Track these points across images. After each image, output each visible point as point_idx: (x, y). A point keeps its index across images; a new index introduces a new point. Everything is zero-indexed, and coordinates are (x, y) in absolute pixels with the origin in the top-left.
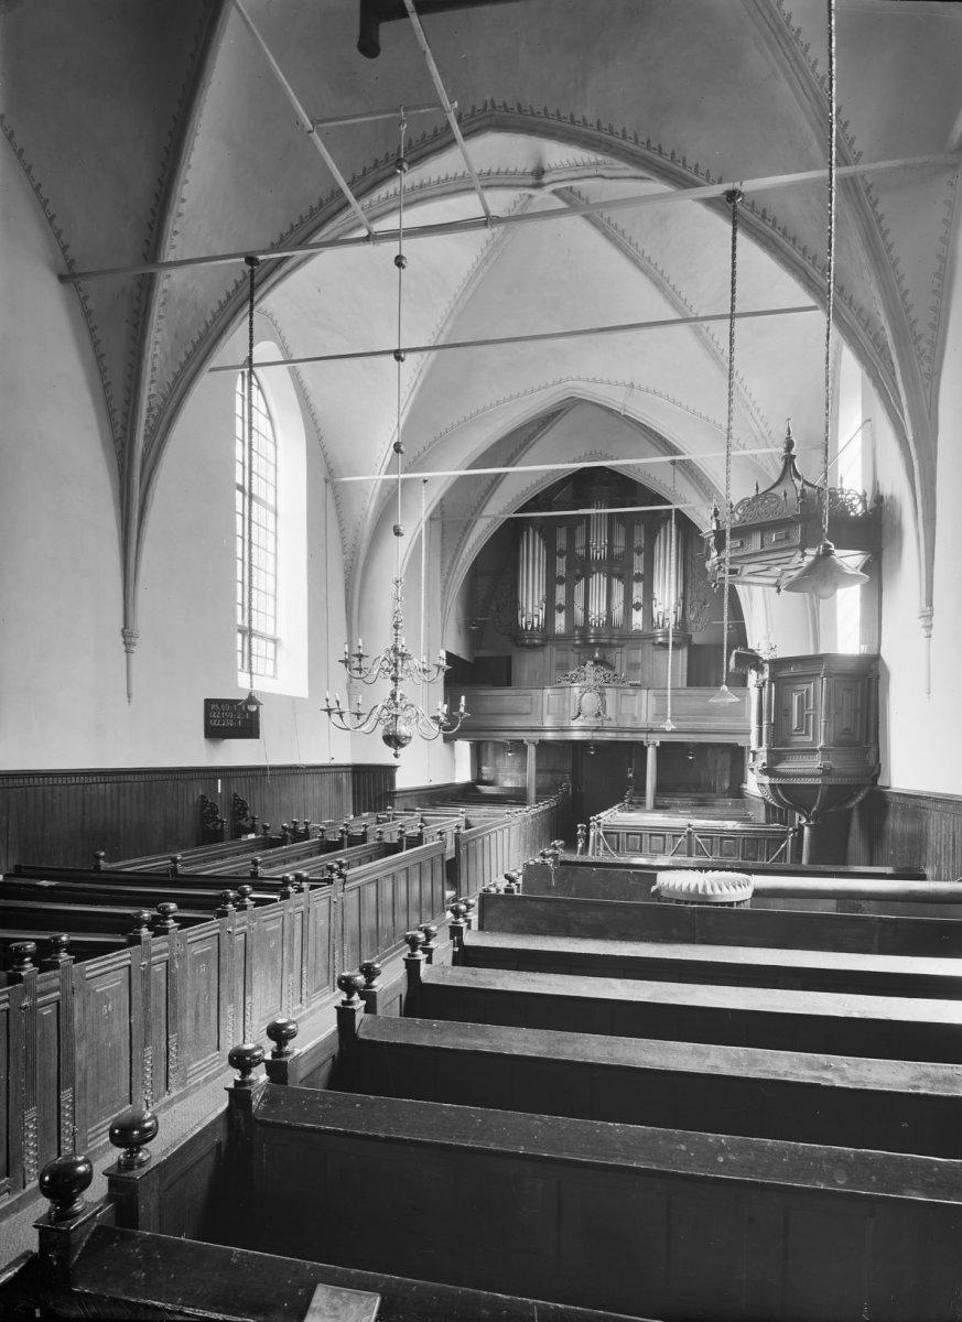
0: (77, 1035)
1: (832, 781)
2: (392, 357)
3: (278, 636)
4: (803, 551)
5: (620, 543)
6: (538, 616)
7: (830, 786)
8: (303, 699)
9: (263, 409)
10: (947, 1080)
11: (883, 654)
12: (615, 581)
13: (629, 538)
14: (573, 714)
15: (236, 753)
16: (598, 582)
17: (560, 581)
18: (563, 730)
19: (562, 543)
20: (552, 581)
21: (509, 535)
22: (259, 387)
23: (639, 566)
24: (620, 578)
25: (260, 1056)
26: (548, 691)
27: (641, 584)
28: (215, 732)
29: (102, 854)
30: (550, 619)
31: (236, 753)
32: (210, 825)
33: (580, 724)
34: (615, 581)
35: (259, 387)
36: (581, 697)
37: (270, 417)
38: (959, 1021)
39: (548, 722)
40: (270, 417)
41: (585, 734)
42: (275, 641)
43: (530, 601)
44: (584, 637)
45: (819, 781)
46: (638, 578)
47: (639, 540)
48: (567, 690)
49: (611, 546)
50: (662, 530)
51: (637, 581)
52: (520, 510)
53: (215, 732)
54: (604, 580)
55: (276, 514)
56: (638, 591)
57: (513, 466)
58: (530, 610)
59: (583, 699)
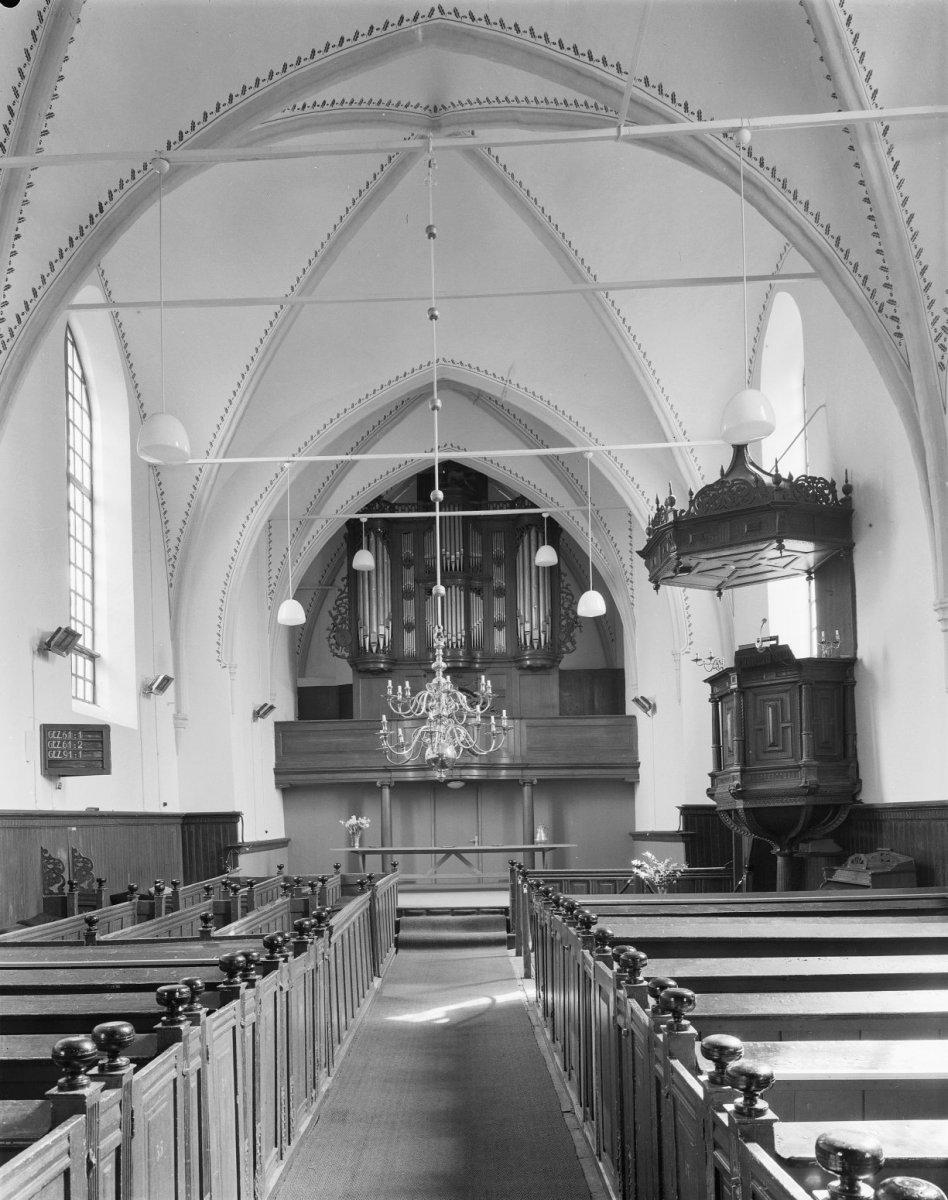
0: (20, 1113)
1: (820, 801)
3: (97, 651)
4: (780, 541)
5: (477, 554)
6: (384, 635)
7: (815, 807)
8: (133, 730)
9: (78, 371)
11: (859, 656)
12: (473, 596)
13: (486, 547)
15: (80, 794)
17: (408, 595)
19: (408, 551)
21: (352, 535)
22: (74, 344)
23: (499, 580)
24: (479, 592)
27: (502, 600)
28: (55, 768)
30: (397, 638)
31: (80, 794)
32: (55, 889)
35: (74, 344)
37: (84, 380)
40: (84, 380)
42: (93, 657)
43: (374, 617)
45: (799, 803)
46: (500, 592)
47: (498, 549)
49: (466, 556)
51: (499, 596)
53: (55, 768)
55: (92, 499)
56: (499, 611)
57: (364, 453)
58: (375, 630)
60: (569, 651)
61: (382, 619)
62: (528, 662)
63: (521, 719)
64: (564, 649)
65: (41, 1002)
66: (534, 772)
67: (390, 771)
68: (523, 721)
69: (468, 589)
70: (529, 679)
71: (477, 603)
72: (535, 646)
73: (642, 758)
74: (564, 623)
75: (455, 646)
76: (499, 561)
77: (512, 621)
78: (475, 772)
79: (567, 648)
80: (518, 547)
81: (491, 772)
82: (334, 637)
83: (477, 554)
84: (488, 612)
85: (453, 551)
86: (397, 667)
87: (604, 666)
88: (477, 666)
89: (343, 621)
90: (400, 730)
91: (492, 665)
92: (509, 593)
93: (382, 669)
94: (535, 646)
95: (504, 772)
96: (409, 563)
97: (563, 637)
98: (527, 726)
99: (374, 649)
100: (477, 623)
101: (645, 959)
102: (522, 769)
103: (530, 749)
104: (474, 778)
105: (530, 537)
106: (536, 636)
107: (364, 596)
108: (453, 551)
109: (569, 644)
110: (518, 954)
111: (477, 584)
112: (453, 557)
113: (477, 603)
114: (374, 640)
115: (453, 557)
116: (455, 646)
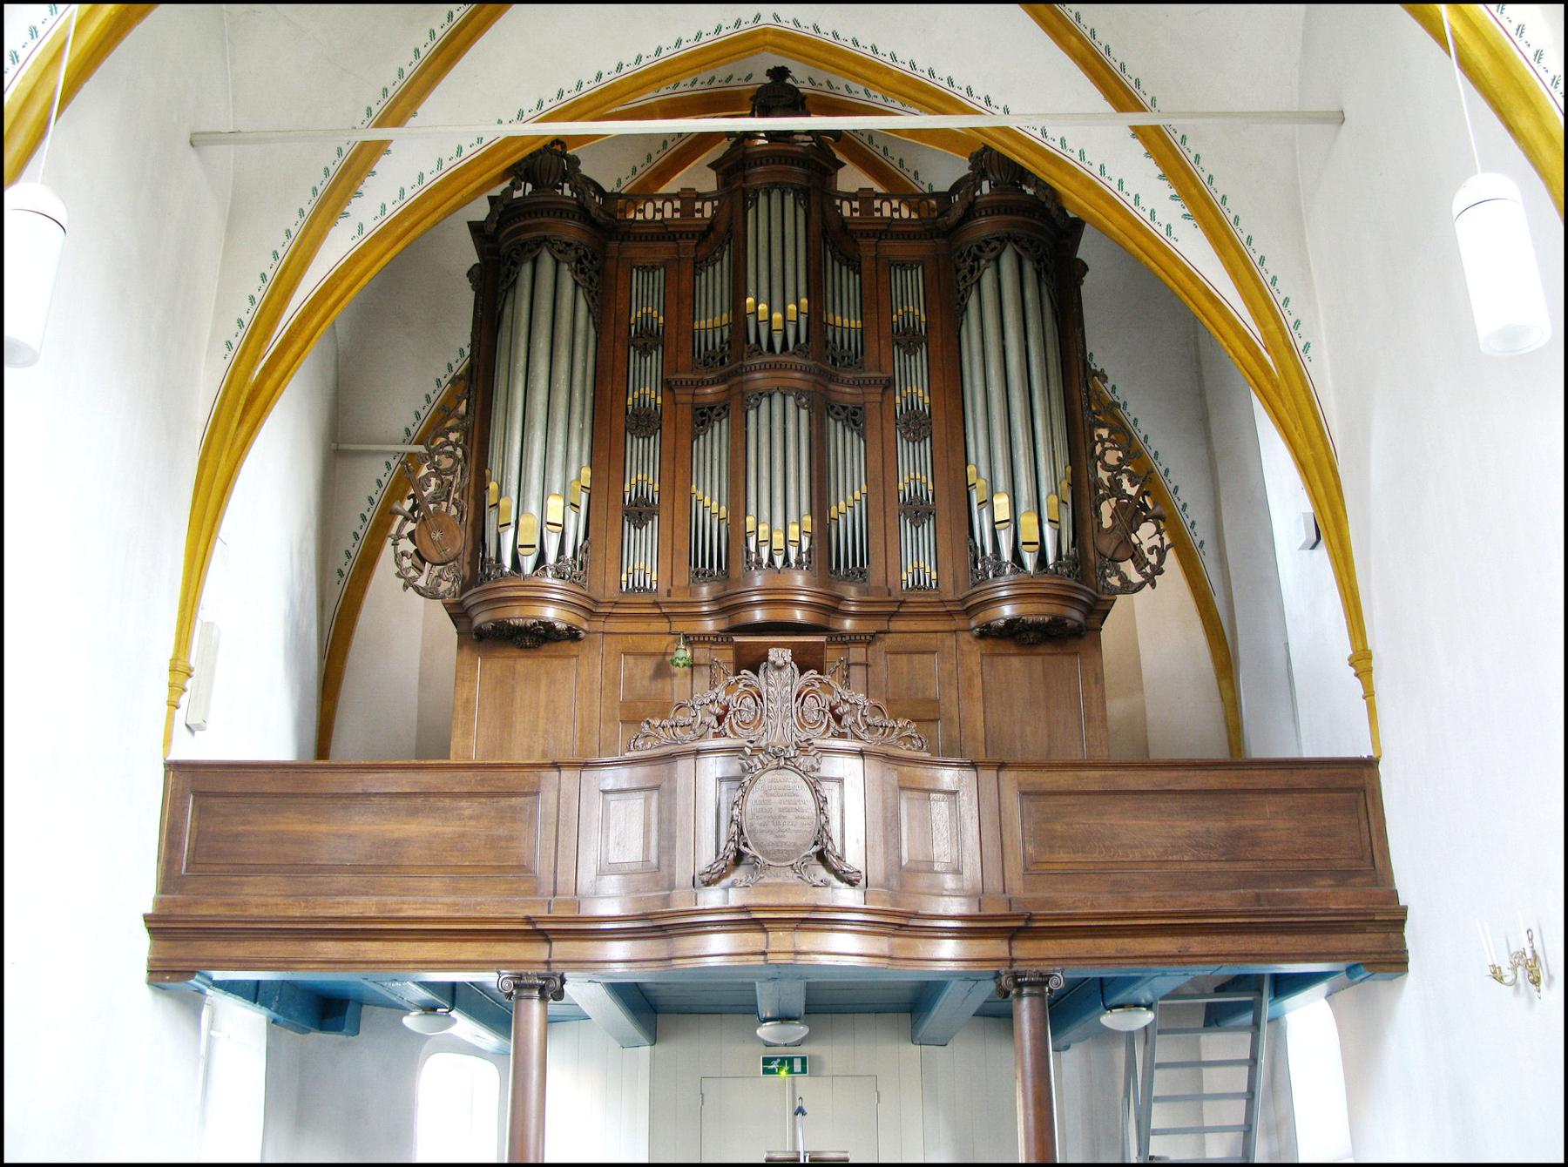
5: (844, 320)
13: (873, 302)
17: (644, 422)
24: (854, 418)
46: (916, 425)
60: (1128, 588)
61: (557, 486)
62: (1007, 611)
63: (1001, 766)
64: (1114, 581)
66: (1050, 947)
67: (545, 936)
68: (1008, 776)
69: (823, 409)
70: (1017, 667)
71: (849, 453)
73: (1410, 875)
74: (1106, 509)
75: (779, 560)
76: (908, 340)
77: (952, 505)
79: (1123, 578)
80: (964, 299)
82: (411, 535)
84: (882, 474)
85: (777, 302)
86: (598, 625)
88: (848, 624)
89: (443, 494)
90: (1147, 1017)
91: (897, 625)
92: (945, 426)
93: (549, 626)
94: (1030, 560)
96: (647, 340)
97: (1107, 545)
98: (1023, 794)
99: (528, 563)
100: (848, 501)
101: (514, 186)
103: (1032, 869)
108: (777, 302)
109: (1128, 567)
110: (1119, 459)
111: (846, 394)
112: (777, 316)
113: (849, 453)
114: (529, 536)
115: (777, 316)
116: (779, 560)
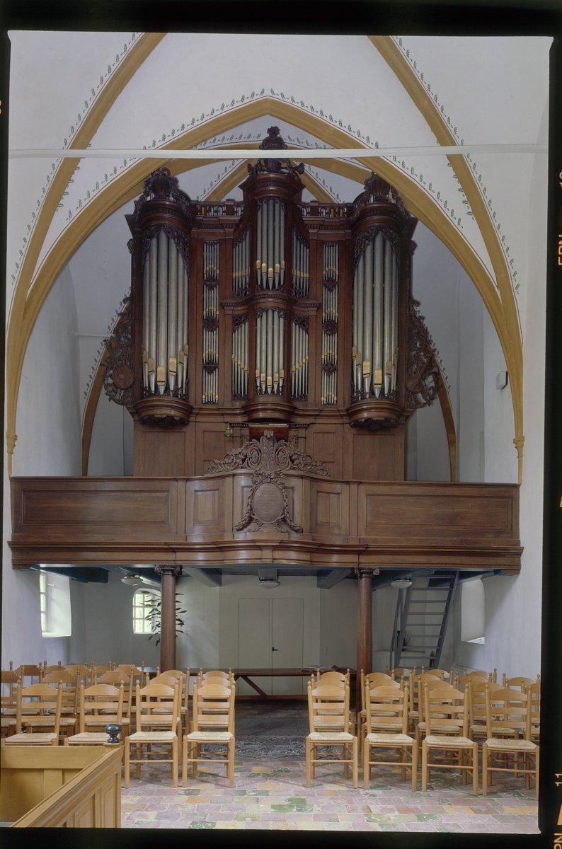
2: (61, 773)
10: (142, 807)
12: (297, 332)
13: (315, 263)
14: (238, 520)
16: (270, 328)
17: (211, 324)
18: (220, 548)
20: (199, 323)
23: (332, 308)
24: (304, 324)
25: (418, 402)
26: (196, 485)
29: (558, 784)
33: (250, 537)
34: (297, 332)
36: (253, 492)
38: (2, 719)
39: (197, 537)
41: (257, 553)
44: (248, 411)
46: (331, 327)
48: (229, 480)
50: (369, 250)
52: (171, 146)
54: (279, 324)
59: (257, 494)
63: (360, 483)
65: (238, 818)
66: (374, 558)
67: (174, 550)
68: (362, 487)
70: (368, 441)
71: (300, 339)
72: (377, 393)
76: (330, 284)
77: (344, 365)
78: (293, 555)
81: (317, 557)
83: (301, 274)
84: (315, 349)
87: (92, 827)
91: (320, 420)
94: (377, 393)
95: (335, 558)
96: (212, 282)
97: (411, 384)
99: (162, 390)
102: (360, 553)
104: (293, 563)
105: (374, 248)
106: (378, 379)
107: (150, 278)
115: (271, 269)
